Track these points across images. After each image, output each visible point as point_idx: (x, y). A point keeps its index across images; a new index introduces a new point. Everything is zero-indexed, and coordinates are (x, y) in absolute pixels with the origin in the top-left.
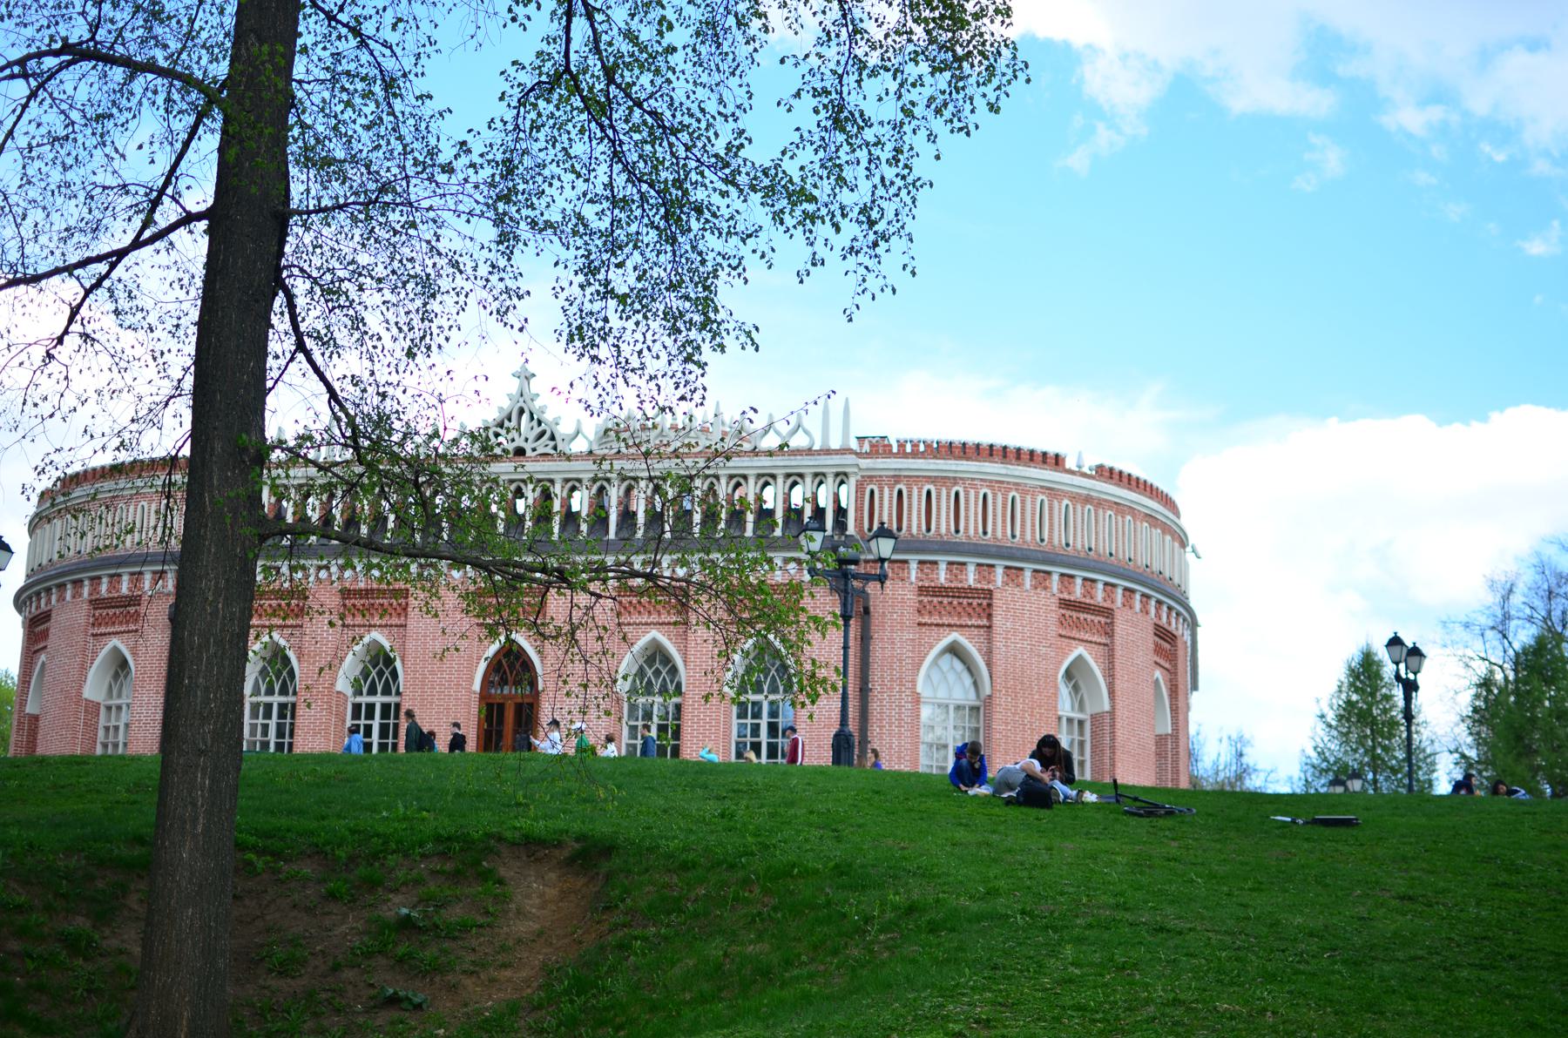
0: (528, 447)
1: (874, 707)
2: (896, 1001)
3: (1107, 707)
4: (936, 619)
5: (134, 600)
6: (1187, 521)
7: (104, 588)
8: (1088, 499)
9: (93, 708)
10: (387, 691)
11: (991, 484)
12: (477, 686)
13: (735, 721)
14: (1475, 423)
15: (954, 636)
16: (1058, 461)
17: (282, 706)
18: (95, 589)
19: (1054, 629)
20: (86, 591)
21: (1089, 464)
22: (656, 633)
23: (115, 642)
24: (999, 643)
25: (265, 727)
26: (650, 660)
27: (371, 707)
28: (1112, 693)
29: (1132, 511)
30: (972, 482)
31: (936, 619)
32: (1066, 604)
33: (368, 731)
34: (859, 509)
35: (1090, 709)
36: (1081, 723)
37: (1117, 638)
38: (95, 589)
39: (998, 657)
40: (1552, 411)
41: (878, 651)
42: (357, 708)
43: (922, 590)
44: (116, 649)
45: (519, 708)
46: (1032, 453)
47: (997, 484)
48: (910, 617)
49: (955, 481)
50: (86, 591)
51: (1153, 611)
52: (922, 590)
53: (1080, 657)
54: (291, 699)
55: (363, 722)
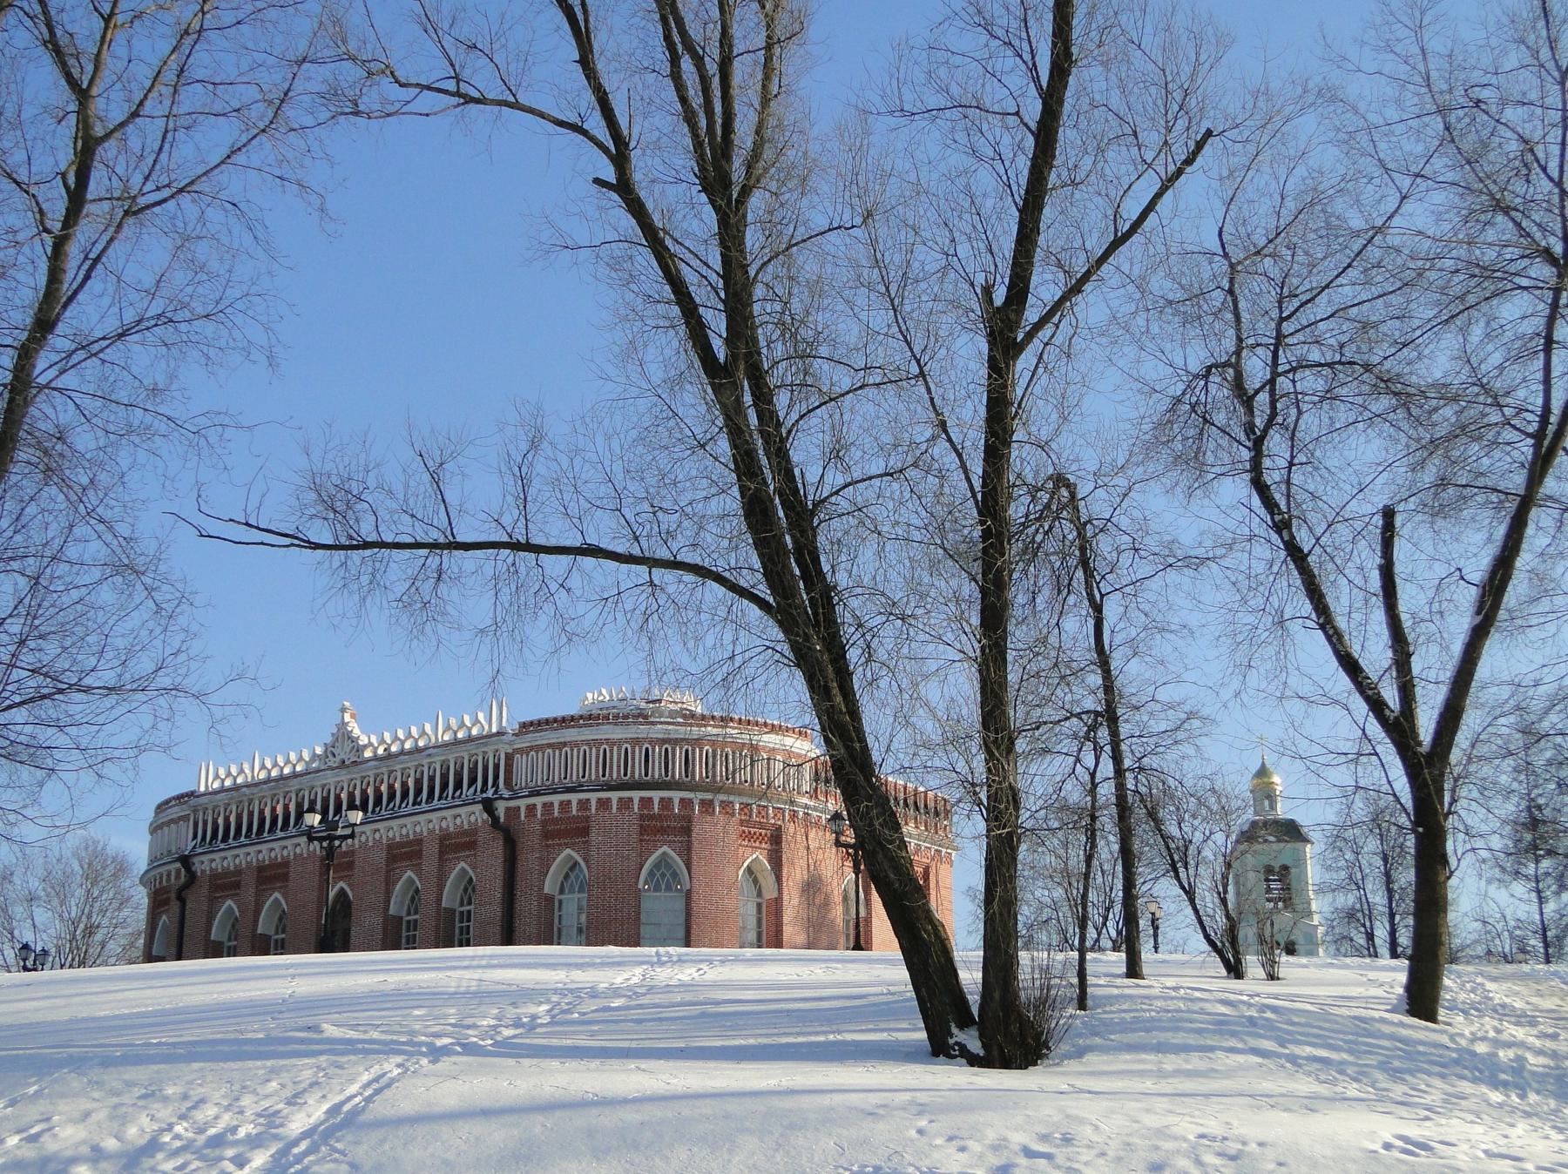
11: (588, 743)
49: (565, 744)
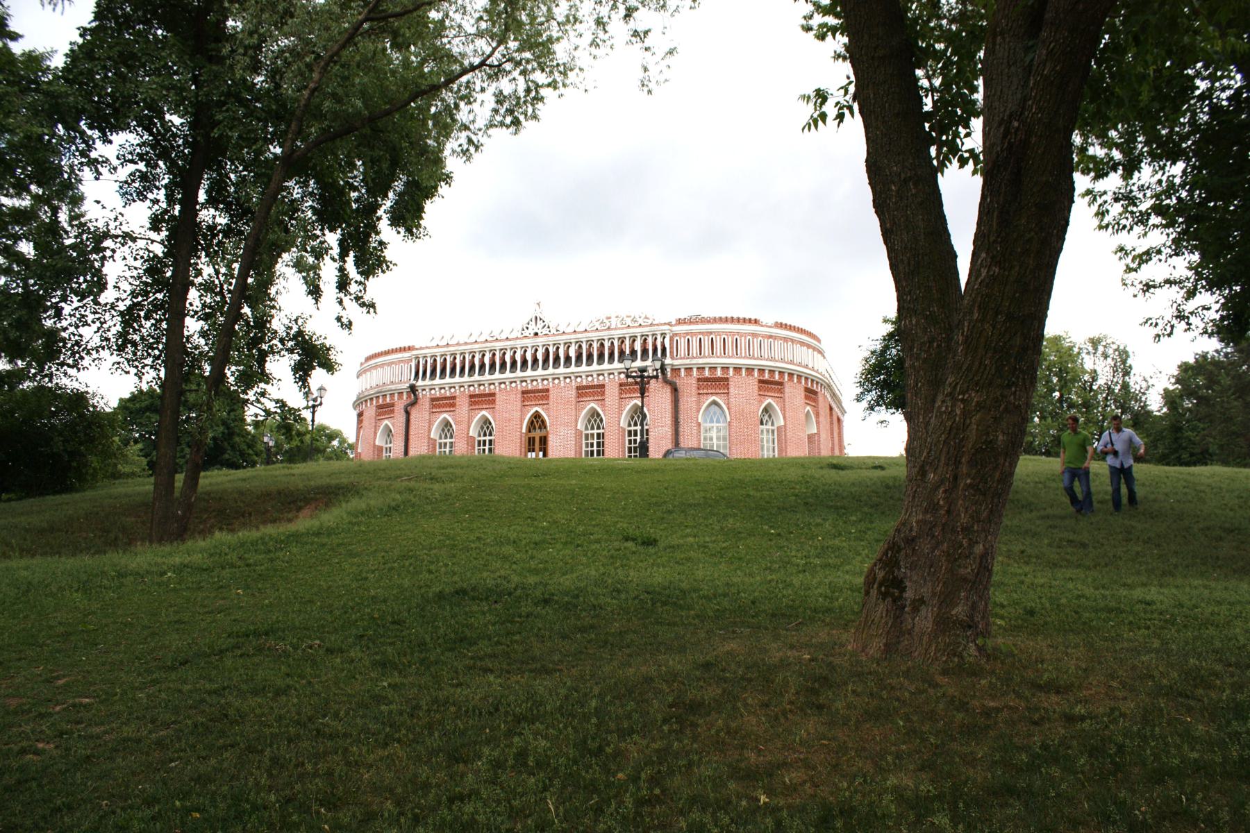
0: (539, 332)
1: (681, 429)
2: (319, 638)
3: (782, 423)
4: (705, 391)
5: (393, 405)
6: (823, 346)
7: (381, 401)
8: (770, 337)
9: (380, 449)
10: (598, 428)
11: (726, 333)
12: (524, 431)
13: (477, 448)
14: (1191, 360)
15: (714, 398)
16: (756, 322)
17: (598, 435)
18: (377, 402)
19: (756, 392)
20: (374, 402)
21: (771, 322)
22: (593, 405)
23: (386, 422)
24: (732, 400)
25: (484, 450)
26: (592, 416)
27: (485, 441)
28: (784, 418)
29: (792, 341)
30: (718, 333)
31: (705, 391)
32: (761, 381)
33: (592, 445)
34: (671, 348)
35: (776, 425)
36: (773, 431)
37: (786, 395)
38: (377, 402)
39: (732, 406)
40: (1049, 313)
41: (682, 406)
42: (630, 432)
43: (699, 380)
44: (387, 425)
45: (541, 438)
46: (744, 319)
47: (732, 333)
48: (694, 391)
49: (711, 333)
50: (374, 402)
51: (803, 381)
52: (699, 380)
53: (769, 404)
54: (601, 431)
55: (633, 438)
